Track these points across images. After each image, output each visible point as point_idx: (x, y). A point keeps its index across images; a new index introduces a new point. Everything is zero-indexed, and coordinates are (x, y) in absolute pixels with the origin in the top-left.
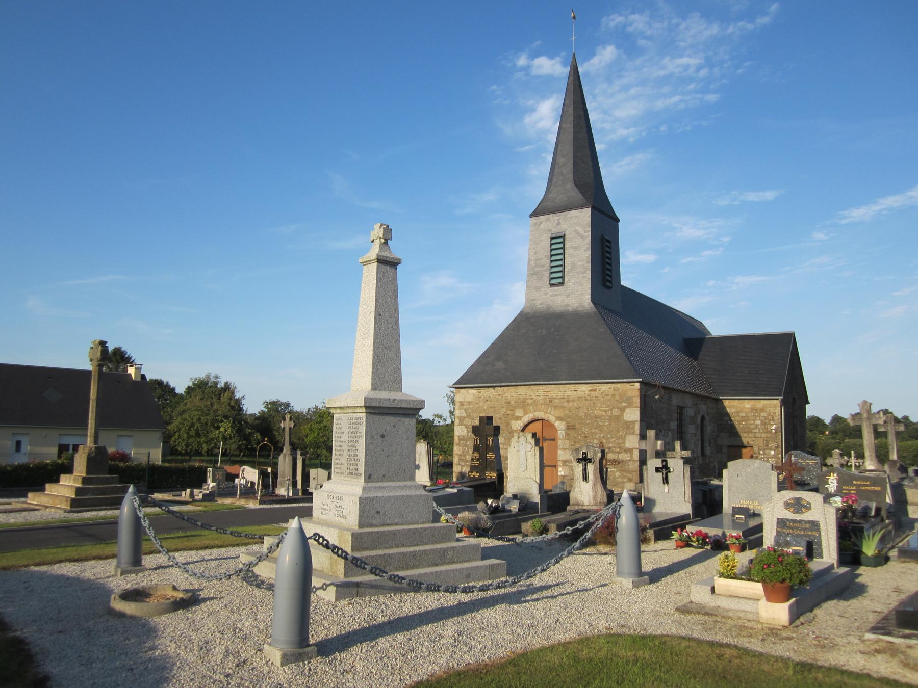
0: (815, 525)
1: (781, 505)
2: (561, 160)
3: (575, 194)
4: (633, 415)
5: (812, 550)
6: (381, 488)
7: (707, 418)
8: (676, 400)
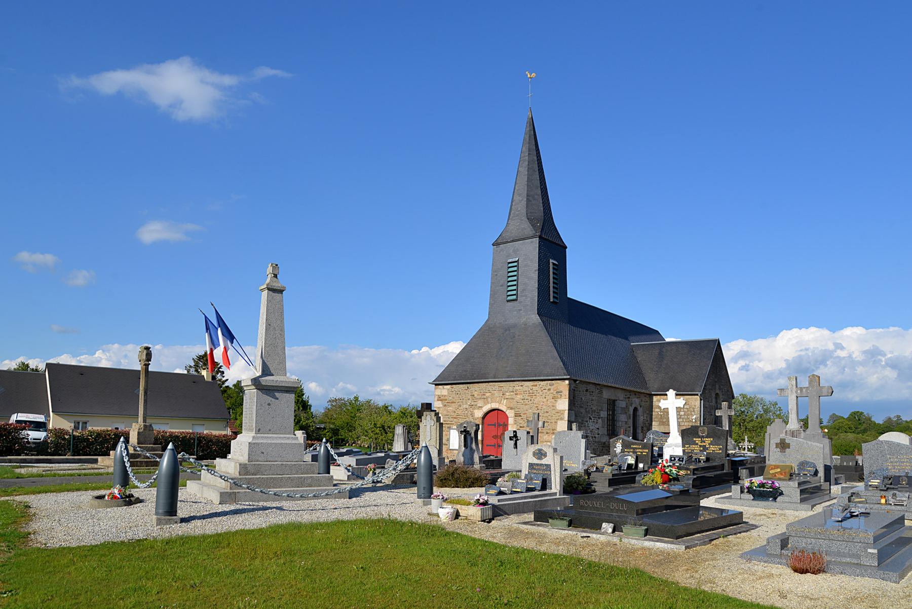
0: (548, 466)
1: (531, 454)
2: (517, 198)
3: (528, 229)
4: (563, 404)
5: (545, 485)
6: (525, 498)
7: (640, 410)
8: (606, 394)
